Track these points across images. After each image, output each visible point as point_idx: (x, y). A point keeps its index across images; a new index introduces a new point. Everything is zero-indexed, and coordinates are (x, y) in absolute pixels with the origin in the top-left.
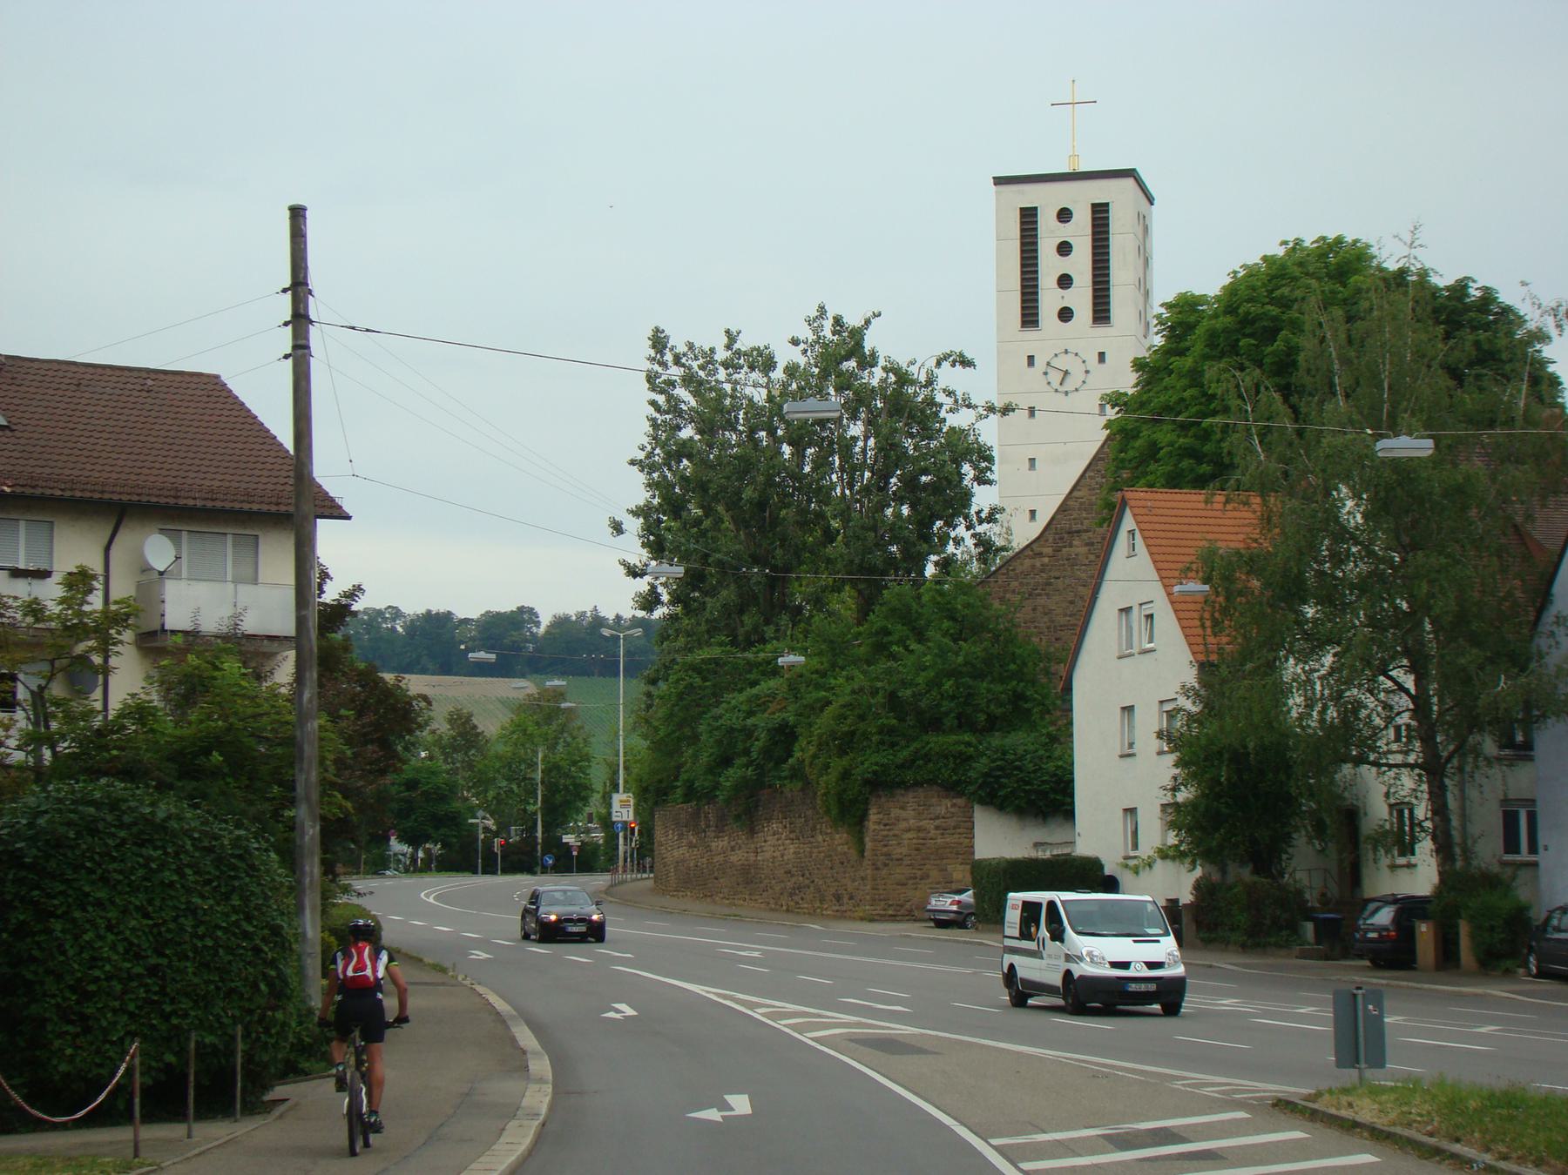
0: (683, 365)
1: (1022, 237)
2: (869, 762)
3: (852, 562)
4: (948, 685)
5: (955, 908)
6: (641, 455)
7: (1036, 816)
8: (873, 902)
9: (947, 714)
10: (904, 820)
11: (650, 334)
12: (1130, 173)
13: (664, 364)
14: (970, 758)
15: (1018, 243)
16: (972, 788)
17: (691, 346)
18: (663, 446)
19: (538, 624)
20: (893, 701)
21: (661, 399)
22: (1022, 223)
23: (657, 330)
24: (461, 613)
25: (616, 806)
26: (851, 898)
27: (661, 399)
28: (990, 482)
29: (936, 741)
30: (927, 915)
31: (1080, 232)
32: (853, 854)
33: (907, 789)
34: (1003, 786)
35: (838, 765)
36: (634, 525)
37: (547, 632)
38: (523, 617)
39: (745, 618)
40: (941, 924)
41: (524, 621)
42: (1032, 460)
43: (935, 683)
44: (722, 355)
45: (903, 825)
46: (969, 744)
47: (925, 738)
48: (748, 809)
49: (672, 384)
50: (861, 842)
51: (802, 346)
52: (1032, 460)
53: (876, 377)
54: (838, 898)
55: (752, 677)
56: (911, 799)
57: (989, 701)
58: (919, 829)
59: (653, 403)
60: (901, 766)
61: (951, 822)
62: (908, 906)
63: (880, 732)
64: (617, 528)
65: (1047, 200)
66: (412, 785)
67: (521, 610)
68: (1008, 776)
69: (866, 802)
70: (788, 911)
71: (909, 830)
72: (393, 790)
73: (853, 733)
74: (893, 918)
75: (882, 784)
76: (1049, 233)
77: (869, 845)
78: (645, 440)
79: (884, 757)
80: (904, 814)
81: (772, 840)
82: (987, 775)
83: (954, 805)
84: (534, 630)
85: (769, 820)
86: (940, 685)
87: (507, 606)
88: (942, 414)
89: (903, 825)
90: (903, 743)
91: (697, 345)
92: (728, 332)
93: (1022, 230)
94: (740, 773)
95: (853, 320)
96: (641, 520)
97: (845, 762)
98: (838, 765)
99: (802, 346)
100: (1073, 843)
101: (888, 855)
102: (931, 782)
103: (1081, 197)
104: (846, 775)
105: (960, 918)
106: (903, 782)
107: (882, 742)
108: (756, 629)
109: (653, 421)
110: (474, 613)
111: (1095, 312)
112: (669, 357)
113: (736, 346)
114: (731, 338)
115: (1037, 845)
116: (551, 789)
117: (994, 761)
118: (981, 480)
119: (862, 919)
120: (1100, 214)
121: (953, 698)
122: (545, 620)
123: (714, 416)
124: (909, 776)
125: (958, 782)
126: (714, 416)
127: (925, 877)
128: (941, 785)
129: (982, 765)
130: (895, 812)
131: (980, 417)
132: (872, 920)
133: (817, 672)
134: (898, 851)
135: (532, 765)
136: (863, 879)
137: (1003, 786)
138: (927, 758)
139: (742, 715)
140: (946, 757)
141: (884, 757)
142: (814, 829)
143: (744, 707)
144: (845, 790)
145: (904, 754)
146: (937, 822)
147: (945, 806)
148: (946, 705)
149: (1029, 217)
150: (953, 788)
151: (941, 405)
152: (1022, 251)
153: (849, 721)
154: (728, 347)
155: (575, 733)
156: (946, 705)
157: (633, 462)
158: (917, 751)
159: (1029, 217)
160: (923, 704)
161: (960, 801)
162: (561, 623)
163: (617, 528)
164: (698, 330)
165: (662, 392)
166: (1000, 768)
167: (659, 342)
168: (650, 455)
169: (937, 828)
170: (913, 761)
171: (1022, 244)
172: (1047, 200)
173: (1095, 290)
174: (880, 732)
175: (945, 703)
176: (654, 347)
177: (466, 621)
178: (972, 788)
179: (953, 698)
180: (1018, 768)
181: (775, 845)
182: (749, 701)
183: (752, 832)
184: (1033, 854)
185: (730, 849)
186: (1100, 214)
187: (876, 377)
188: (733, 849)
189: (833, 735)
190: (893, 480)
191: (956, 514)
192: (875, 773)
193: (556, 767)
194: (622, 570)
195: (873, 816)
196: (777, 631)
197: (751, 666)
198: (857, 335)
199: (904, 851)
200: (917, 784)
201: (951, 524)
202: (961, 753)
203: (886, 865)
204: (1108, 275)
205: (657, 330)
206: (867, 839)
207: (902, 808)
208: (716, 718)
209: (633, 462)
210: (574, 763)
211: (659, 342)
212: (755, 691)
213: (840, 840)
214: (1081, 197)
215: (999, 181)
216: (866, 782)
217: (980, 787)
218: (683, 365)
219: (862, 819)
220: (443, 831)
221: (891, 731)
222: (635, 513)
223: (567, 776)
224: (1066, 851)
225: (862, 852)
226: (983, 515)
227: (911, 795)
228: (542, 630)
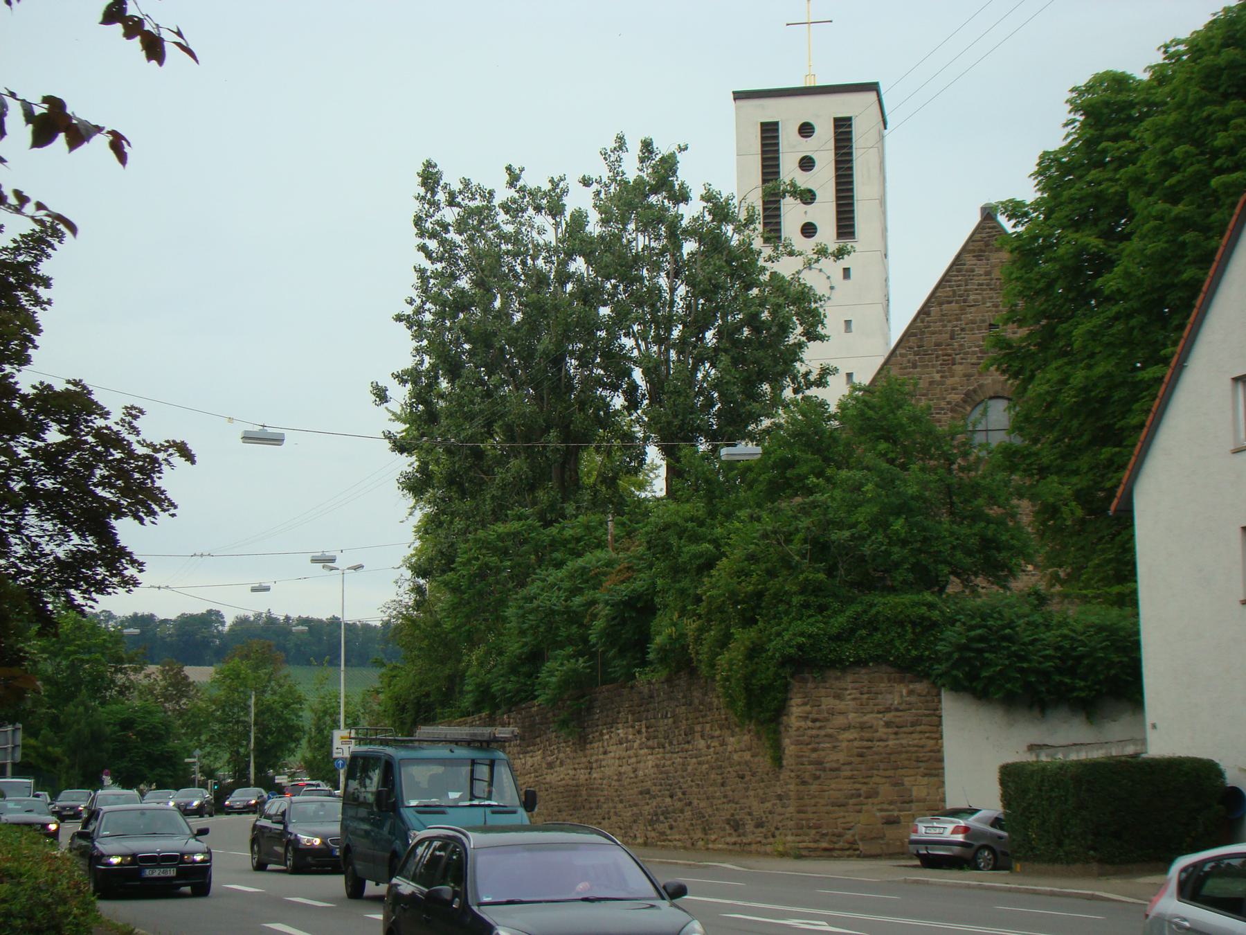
0: (459, 205)
1: (763, 152)
2: (790, 633)
3: (669, 423)
4: (898, 525)
5: (960, 838)
6: (409, 310)
7: (1030, 707)
8: (800, 829)
9: (897, 565)
10: (841, 714)
11: (420, 169)
12: (873, 87)
13: (434, 204)
14: (934, 624)
15: (759, 158)
16: (940, 668)
17: (466, 183)
18: (436, 299)
19: (223, 624)
20: (820, 549)
21: (433, 245)
22: (763, 138)
23: (429, 164)
24: (161, 615)
25: (337, 743)
26: (759, 825)
27: (433, 245)
28: (821, 338)
29: (884, 604)
30: (912, 848)
31: (822, 147)
32: (764, 762)
33: (844, 670)
34: (987, 664)
35: (743, 637)
36: (400, 394)
37: (232, 629)
38: (211, 618)
39: (540, 494)
40: (931, 862)
41: (213, 621)
42: (848, 323)
43: (879, 523)
44: (503, 194)
45: (839, 721)
46: (931, 606)
47: (867, 599)
48: (578, 714)
49: (445, 227)
50: (777, 747)
51: (595, 187)
52: (848, 323)
53: (691, 211)
54: (736, 826)
55: (558, 555)
56: (848, 683)
57: (954, 548)
58: (863, 727)
59: (423, 248)
60: (837, 638)
61: (908, 717)
62: (848, 835)
63: (802, 592)
64: (381, 395)
65: (788, 114)
66: (127, 724)
67: (210, 612)
68: (992, 649)
69: (786, 688)
70: (645, 844)
71: (847, 728)
72: (108, 730)
73: (759, 595)
74: (828, 853)
75: (809, 663)
76: (791, 148)
77: (790, 748)
78: (414, 294)
79: (813, 625)
80: (840, 705)
81: (616, 751)
82: (961, 648)
83: (911, 693)
84: (220, 628)
85: (612, 724)
86: (886, 525)
87: (198, 609)
88: (761, 263)
89: (839, 721)
90: (836, 605)
91: (474, 182)
92: (509, 169)
93: (763, 145)
94: (568, 665)
95: (663, 148)
96: (409, 386)
97: (752, 633)
98: (743, 637)
99: (595, 187)
100: (1144, 741)
101: (819, 763)
102: (879, 660)
103: (823, 112)
104: (754, 652)
105: (969, 853)
106: (841, 661)
107: (806, 606)
108: (552, 506)
109: (421, 272)
110: (173, 615)
111: (839, 227)
112: (441, 196)
113: (520, 183)
114: (514, 178)
115: (1032, 748)
116: (263, 730)
117: (972, 628)
118: (812, 335)
119: (783, 855)
120: (843, 127)
121: (904, 543)
122: (229, 620)
123: (489, 270)
124: (848, 651)
125: (920, 659)
126: (489, 270)
127: (872, 794)
128: (891, 664)
129: (953, 635)
130: (828, 702)
131: (808, 265)
132: (799, 857)
133: (692, 519)
134: (832, 758)
135: (246, 708)
136: (780, 797)
137: (987, 664)
138: (873, 626)
139: (563, 595)
140: (901, 624)
141: (813, 625)
142: (690, 732)
143: (567, 585)
144: (753, 673)
145: (840, 621)
146: (889, 716)
147: (898, 693)
148: (897, 553)
149: (770, 132)
150: (910, 669)
151: (760, 253)
152: (763, 167)
153: (755, 578)
154: (511, 184)
155: (282, 681)
156: (897, 553)
157: (399, 318)
158: (858, 616)
159: (770, 132)
160: (866, 549)
161: (921, 687)
162: (242, 622)
163: (381, 395)
164: (477, 166)
165: (433, 235)
166: (981, 639)
167: (430, 178)
168: (420, 310)
169: (887, 724)
170: (853, 631)
171: (763, 159)
172: (788, 114)
173: (838, 206)
174: (802, 592)
175: (896, 549)
176: (424, 184)
177: (165, 621)
178: (940, 668)
179: (904, 543)
180: (1006, 638)
181: (622, 755)
182: (571, 576)
183: (582, 742)
184: (1031, 758)
185: (558, 767)
186: (843, 127)
187: (691, 211)
188: (550, 766)
189: (733, 597)
190: (709, 335)
191: (783, 374)
192: (800, 647)
193: (269, 709)
194: (387, 444)
195: (796, 708)
196: (578, 508)
197: (554, 544)
198: (668, 165)
199: (842, 757)
200: (860, 663)
201: (778, 388)
202: (922, 618)
203: (817, 778)
204: (852, 190)
205: (429, 164)
206: (786, 741)
207: (838, 697)
208: (530, 599)
209: (399, 318)
210: (287, 706)
211: (430, 178)
212: (580, 562)
213: (740, 744)
214: (823, 112)
215: (739, 96)
216: (786, 661)
217: (955, 666)
218: (459, 205)
219: (781, 710)
220: (158, 771)
221: (818, 589)
222: (401, 378)
223: (280, 717)
224: (1130, 750)
225: (778, 760)
226: (812, 378)
227: (849, 678)
228: (226, 629)
